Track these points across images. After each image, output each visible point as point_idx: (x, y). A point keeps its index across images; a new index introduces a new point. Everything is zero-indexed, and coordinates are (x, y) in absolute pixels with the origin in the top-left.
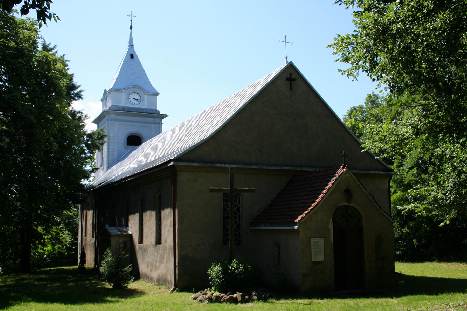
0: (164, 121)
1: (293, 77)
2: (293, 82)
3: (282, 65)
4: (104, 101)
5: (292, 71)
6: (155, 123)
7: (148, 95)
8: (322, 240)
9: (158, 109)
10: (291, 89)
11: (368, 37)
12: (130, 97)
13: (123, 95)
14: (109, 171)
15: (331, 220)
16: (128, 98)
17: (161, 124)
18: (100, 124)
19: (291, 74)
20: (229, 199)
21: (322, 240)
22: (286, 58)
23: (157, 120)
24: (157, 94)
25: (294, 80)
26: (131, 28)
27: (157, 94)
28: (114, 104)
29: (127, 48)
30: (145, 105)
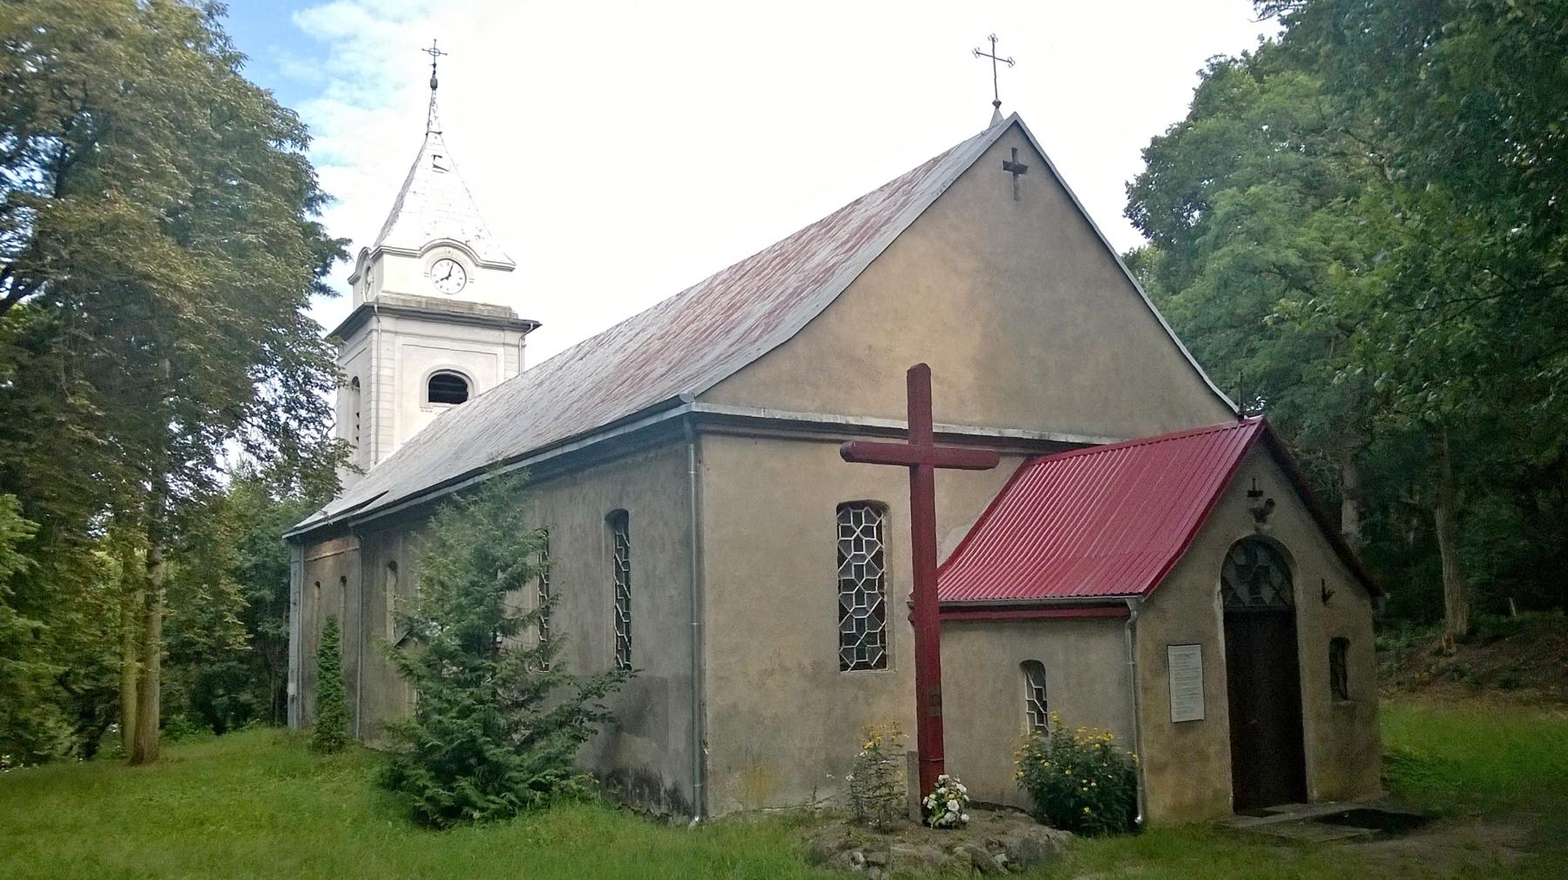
3: (975, 122)
8: (1197, 650)
15: (1219, 587)
22: (997, 104)
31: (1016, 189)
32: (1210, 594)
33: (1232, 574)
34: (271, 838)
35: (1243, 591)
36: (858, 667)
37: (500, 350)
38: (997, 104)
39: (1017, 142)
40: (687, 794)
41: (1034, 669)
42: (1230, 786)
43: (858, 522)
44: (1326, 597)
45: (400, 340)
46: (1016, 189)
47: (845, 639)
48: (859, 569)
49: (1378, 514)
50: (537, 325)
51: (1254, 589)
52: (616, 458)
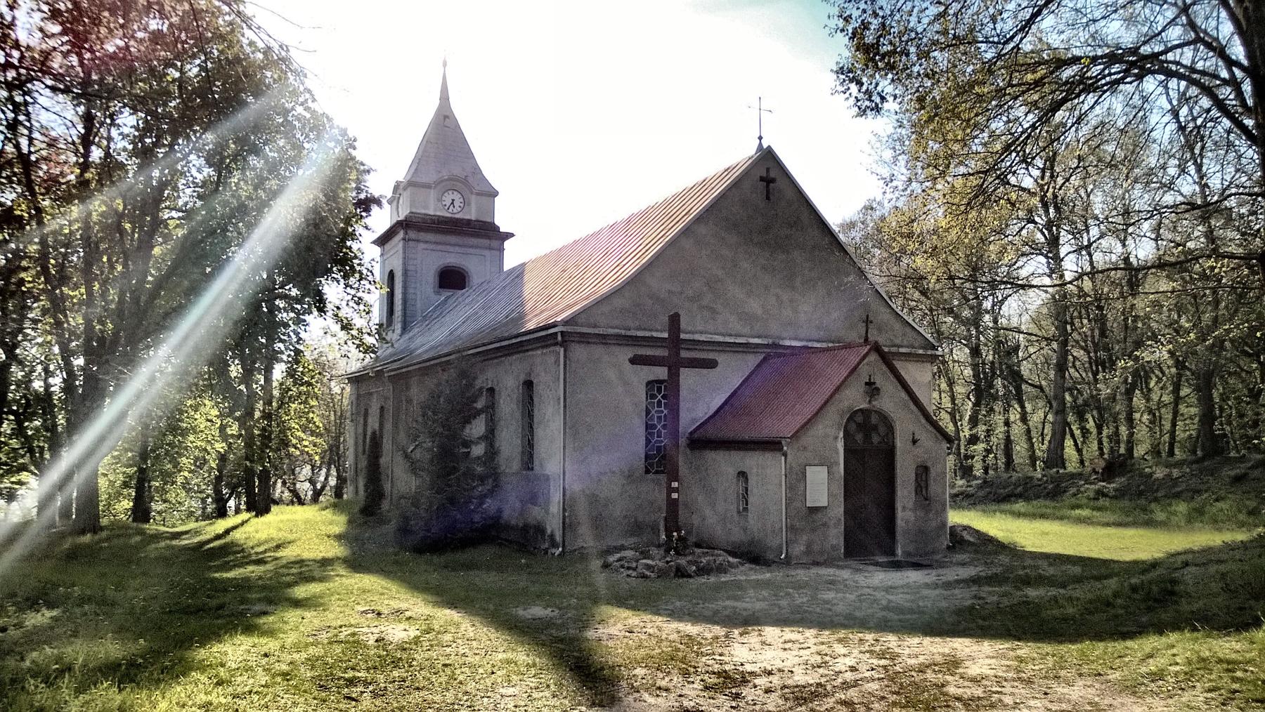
0: (507, 244)
1: (772, 175)
2: (771, 185)
3: (742, 152)
4: (395, 203)
5: (770, 164)
6: (490, 248)
7: (478, 194)
8: (825, 468)
9: (496, 223)
10: (768, 198)
11: (67, 231)
12: (444, 198)
13: (432, 194)
14: (407, 337)
15: (841, 435)
16: (440, 200)
17: (501, 250)
18: (387, 246)
19: (768, 170)
20: (899, 558)
21: (825, 468)
22: (760, 138)
23: (495, 243)
24: (495, 194)
25: (773, 181)
26: (445, 64)
27: (495, 194)
28: (414, 210)
29: (437, 102)
30: (471, 214)
31: (768, 192)
32: (836, 438)
33: (853, 427)
34: (736, 645)
35: (859, 437)
36: (657, 472)
37: (487, 253)
38: (760, 138)
39: (770, 164)
40: (558, 538)
41: (743, 475)
42: (842, 543)
43: (659, 390)
44: (914, 442)
45: (422, 246)
46: (768, 192)
47: (647, 457)
48: (659, 418)
49: (1146, 356)
50: (512, 235)
51: (867, 437)
52: (528, 351)
